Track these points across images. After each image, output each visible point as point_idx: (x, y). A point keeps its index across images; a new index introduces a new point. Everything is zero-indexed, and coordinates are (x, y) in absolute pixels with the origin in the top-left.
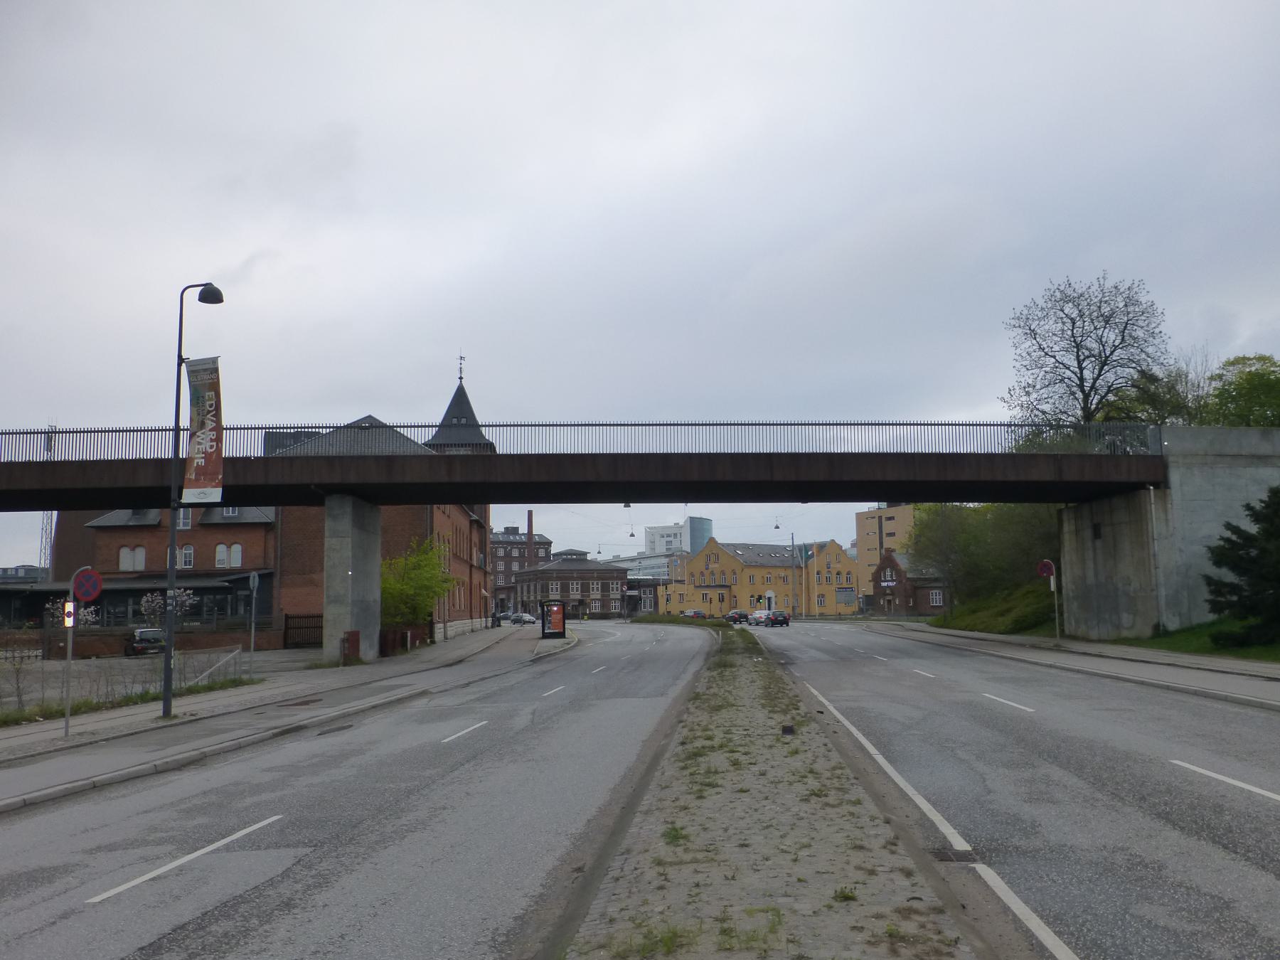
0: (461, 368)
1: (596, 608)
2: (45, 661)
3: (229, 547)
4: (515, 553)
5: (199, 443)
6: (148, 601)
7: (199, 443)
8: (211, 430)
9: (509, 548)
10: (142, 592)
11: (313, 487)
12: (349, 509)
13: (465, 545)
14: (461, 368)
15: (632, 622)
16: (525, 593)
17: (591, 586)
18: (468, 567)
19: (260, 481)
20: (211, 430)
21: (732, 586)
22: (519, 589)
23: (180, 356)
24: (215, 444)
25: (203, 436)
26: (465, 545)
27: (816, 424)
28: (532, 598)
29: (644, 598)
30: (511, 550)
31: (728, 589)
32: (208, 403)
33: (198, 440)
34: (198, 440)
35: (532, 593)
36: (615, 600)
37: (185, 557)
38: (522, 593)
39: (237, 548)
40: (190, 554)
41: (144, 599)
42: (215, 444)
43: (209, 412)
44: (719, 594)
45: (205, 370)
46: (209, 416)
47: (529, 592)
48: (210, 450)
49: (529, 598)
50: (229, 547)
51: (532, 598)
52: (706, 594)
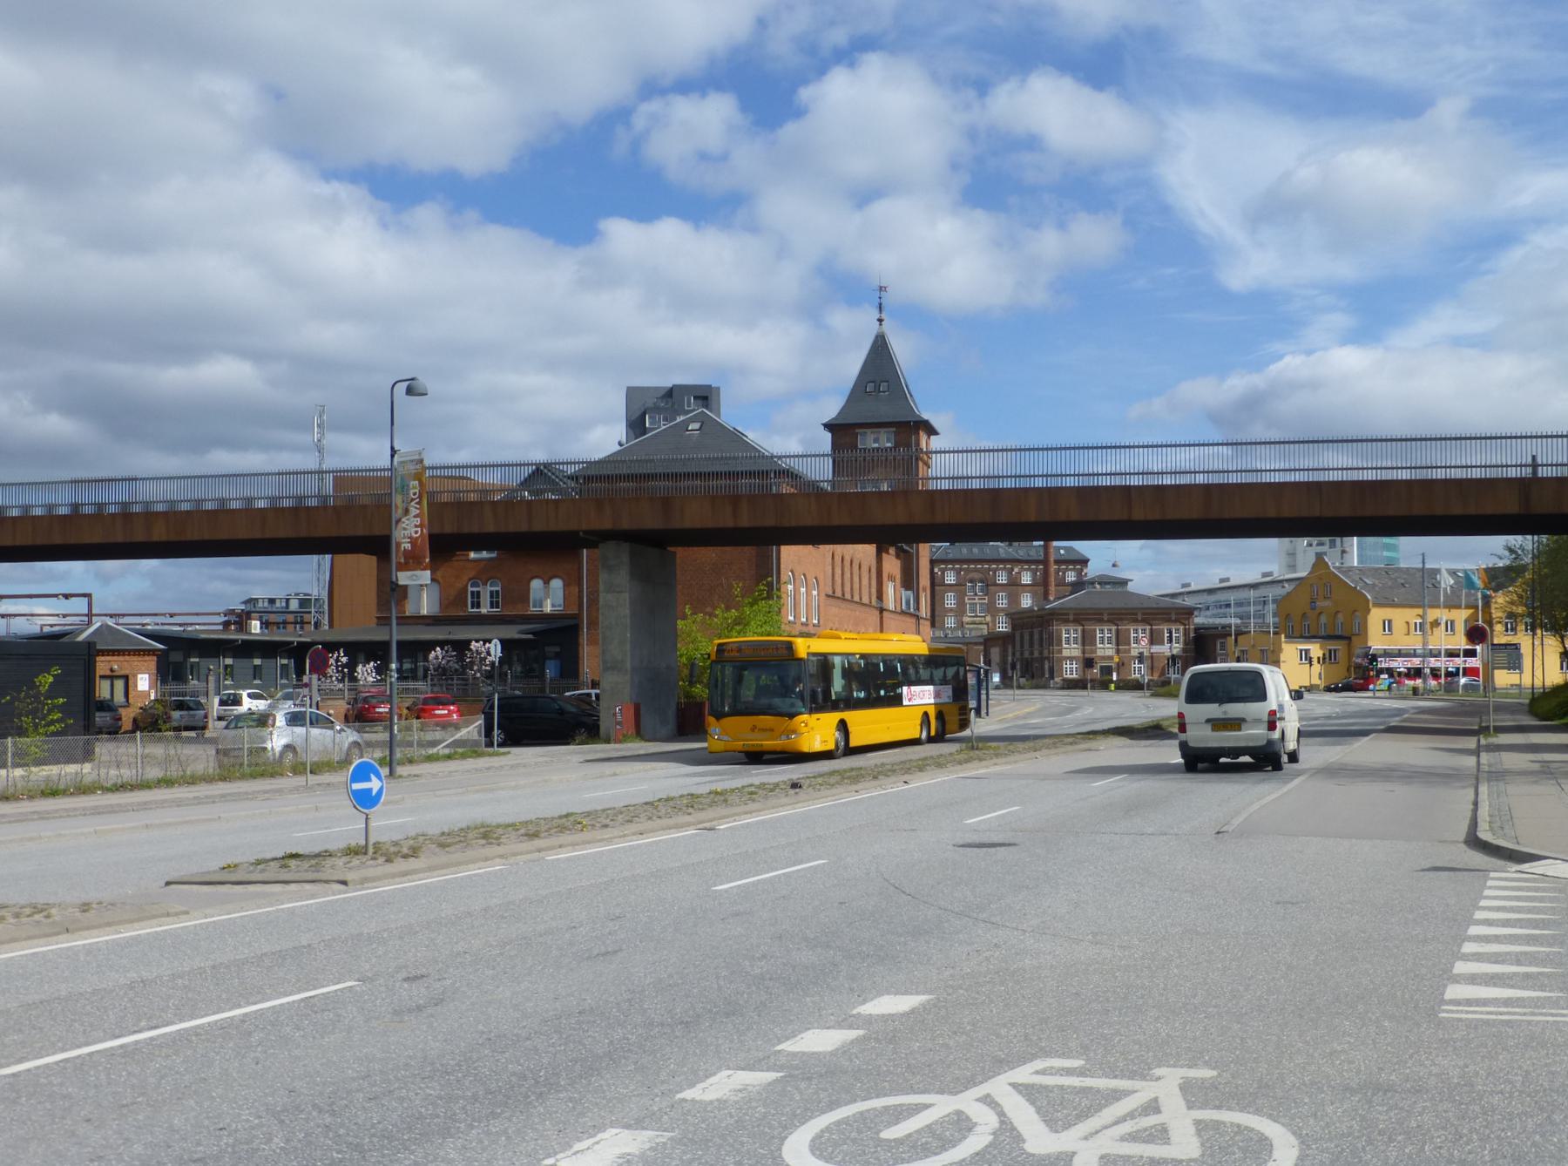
0: (880, 304)
1: (1071, 670)
2: (1025, 1137)
3: (547, 582)
4: (1026, 579)
5: (405, 529)
6: (437, 658)
7: (405, 529)
8: (415, 517)
9: (1016, 570)
10: (430, 645)
11: (581, 534)
12: (625, 558)
13: (865, 581)
14: (880, 304)
15: (1152, 695)
16: (1026, 646)
17: (1132, 635)
18: (877, 613)
19: (524, 527)
20: (415, 517)
21: (1354, 638)
22: (1018, 638)
23: (392, 448)
24: (419, 529)
25: (407, 522)
26: (865, 581)
27: (1166, 446)
28: (1036, 654)
29: (1221, 655)
30: (1019, 573)
31: (1346, 642)
32: (412, 492)
33: (404, 525)
34: (404, 525)
35: (1036, 646)
36: (1071, 659)
37: (491, 597)
38: (1022, 646)
39: (557, 584)
40: (498, 592)
41: (432, 655)
42: (419, 529)
43: (413, 500)
44: (1301, 651)
45: (412, 461)
46: (413, 504)
47: (1031, 645)
48: (415, 536)
49: (1032, 653)
50: (547, 582)
51: (1036, 654)
52: (1335, 651)
